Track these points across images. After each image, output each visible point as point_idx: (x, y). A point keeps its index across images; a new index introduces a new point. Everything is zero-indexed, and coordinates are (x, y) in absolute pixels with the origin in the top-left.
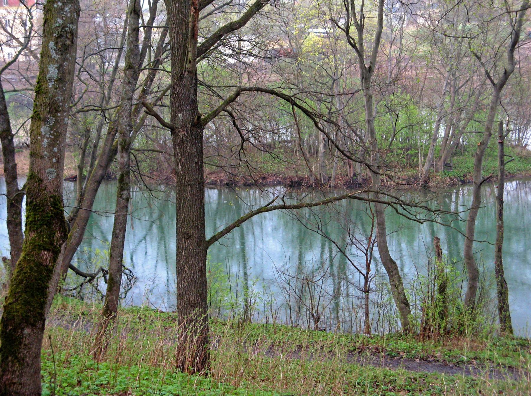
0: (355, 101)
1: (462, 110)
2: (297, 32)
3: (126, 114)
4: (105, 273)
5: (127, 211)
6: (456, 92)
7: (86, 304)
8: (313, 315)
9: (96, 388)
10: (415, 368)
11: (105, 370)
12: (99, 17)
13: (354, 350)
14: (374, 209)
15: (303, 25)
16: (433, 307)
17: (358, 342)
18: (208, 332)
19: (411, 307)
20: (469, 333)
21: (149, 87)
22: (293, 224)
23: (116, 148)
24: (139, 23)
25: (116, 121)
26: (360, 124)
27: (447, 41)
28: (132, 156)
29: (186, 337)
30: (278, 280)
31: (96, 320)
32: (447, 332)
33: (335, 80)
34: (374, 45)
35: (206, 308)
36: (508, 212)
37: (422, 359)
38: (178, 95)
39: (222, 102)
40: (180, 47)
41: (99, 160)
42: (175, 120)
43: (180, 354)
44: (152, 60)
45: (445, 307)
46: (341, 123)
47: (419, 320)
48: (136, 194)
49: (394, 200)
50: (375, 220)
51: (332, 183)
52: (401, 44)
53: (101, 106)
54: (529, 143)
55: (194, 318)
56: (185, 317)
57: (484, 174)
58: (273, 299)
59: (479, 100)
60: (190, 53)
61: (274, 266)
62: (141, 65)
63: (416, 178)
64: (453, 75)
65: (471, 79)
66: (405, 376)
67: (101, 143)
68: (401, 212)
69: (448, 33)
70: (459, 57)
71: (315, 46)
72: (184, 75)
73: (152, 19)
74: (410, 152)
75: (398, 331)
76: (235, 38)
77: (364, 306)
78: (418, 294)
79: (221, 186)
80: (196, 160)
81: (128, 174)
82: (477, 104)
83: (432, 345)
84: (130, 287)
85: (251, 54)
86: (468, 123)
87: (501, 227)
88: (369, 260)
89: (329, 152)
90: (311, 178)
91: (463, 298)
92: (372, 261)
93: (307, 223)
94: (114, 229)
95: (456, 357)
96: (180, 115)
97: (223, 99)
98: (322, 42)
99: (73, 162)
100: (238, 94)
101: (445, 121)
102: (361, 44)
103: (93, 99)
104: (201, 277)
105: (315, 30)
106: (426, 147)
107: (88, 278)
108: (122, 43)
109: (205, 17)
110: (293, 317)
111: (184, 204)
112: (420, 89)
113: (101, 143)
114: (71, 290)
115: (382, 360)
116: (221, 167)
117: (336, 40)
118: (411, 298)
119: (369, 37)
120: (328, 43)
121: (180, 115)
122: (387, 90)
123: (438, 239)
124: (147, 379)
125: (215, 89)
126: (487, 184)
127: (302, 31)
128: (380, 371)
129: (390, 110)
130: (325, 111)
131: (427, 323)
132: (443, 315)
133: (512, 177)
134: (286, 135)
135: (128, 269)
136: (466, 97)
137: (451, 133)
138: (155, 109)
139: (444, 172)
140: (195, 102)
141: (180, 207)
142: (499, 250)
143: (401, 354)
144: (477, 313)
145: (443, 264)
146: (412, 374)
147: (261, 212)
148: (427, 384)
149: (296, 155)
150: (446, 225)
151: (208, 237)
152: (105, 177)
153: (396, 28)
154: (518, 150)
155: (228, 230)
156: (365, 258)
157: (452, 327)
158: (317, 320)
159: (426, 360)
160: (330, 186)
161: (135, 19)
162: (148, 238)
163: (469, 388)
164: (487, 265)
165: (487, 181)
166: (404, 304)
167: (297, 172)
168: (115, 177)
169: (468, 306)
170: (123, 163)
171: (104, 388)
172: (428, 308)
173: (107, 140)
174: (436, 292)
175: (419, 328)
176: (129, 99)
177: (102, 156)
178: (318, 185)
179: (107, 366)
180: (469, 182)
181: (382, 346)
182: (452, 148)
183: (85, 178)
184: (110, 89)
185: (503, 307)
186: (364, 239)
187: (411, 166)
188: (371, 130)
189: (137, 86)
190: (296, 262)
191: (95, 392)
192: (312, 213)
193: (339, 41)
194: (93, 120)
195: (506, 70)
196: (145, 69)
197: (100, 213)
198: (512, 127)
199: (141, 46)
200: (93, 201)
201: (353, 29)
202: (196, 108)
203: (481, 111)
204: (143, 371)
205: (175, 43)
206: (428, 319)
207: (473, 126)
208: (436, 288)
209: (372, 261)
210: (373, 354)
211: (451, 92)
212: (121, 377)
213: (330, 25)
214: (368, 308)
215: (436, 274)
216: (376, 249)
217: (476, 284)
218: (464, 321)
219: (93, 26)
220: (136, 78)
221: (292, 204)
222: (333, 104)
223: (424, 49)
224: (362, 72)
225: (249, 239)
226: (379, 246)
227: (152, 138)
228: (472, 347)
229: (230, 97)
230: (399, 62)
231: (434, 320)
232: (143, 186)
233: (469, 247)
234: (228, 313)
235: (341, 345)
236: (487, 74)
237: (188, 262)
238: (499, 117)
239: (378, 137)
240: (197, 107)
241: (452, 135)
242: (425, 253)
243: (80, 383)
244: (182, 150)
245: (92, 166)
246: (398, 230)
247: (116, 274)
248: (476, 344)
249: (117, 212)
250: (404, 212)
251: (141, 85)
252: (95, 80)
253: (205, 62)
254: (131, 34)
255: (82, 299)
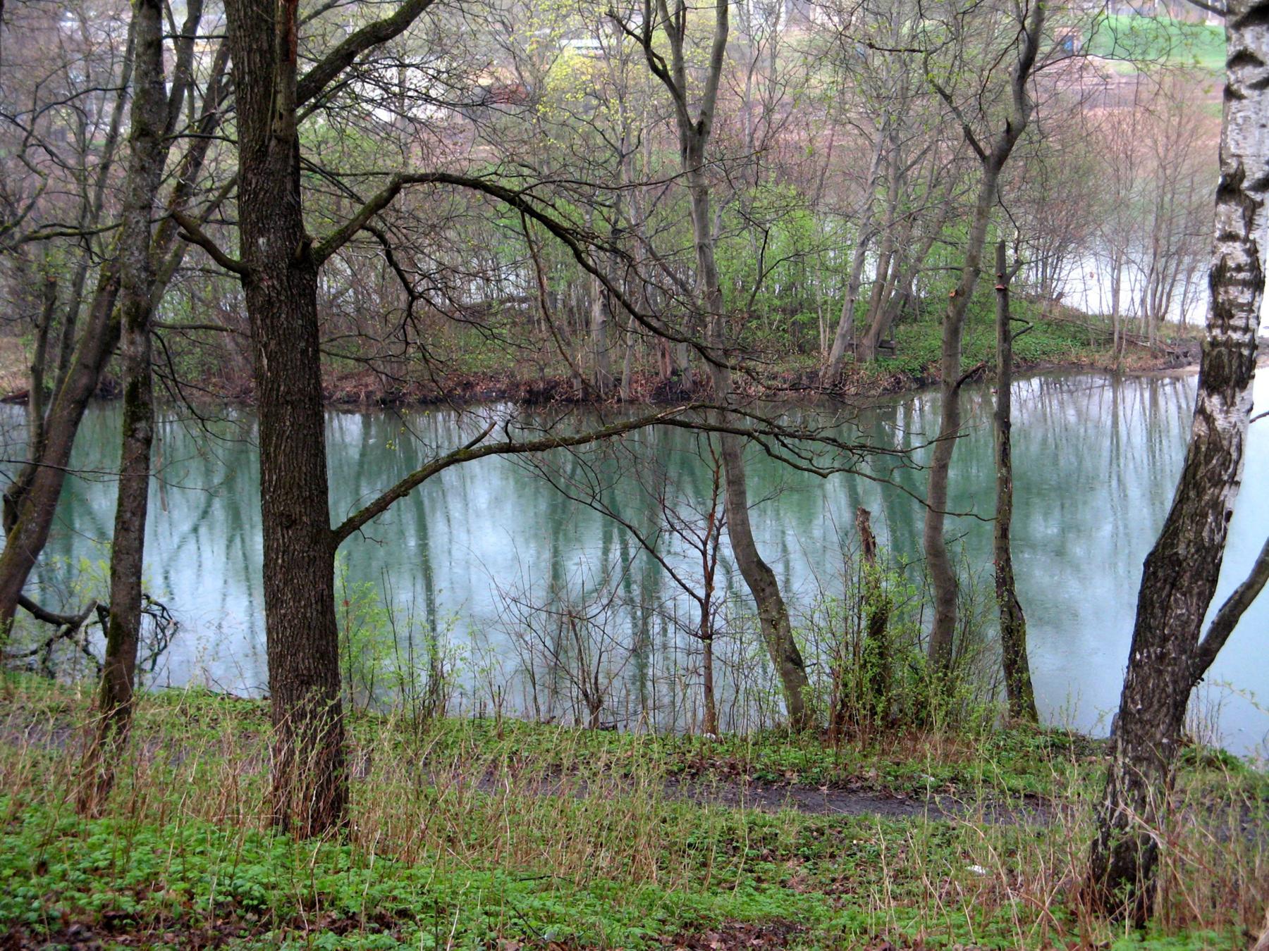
0: (670, 202)
1: (915, 219)
2: (535, 46)
3: (139, 243)
4: (101, 610)
5: (147, 468)
6: (900, 177)
7: (62, 687)
8: (586, 695)
9: (83, 877)
10: (820, 805)
11: (104, 836)
12: (73, 20)
13: (681, 770)
14: (718, 449)
15: (548, 31)
16: (857, 667)
17: (689, 752)
18: (342, 739)
19: (808, 670)
20: (939, 724)
21: (193, 180)
22: (537, 489)
23: (119, 323)
24: (160, 29)
25: (116, 259)
26: (684, 256)
27: (877, 61)
28: (156, 344)
29: (291, 752)
30: (505, 617)
31: (80, 720)
32: (891, 724)
33: (623, 156)
34: (710, 72)
35: (336, 684)
36: (1023, 448)
37: (834, 785)
38: (256, 195)
39: (358, 208)
40: (256, 81)
41: (81, 353)
42: (250, 254)
43: (280, 792)
44: (198, 116)
45: (885, 667)
46: (640, 254)
47: (826, 697)
48: (170, 430)
49: (763, 426)
50: (723, 471)
51: (624, 393)
52: (774, 70)
53: (82, 226)
54: (1066, 290)
55: (308, 709)
56: (288, 707)
57: (965, 363)
58: (494, 661)
59: (953, 195)
60: (279, 96)
61: (493, 585)
62: (170, 126)
63: (813, 375)
64: (892, 139)
65: (933, 148)
66: (797, 823)
67: (84, 311)
68: (777, 453)
69: (877, 42)
70: (904, 97)
71: (576, 79)
72: (268, 146)
73: (194, 19)
74: (798, 317)
75: (779, 724)
76: (389, 62)
77: (702, 671)
78: (823, 640)
79: (368, 405)
80: (303, 344)
81: (147, 382)
82: (947, 203)
83: (856, 754)
84: (163, 644)
85: (428, 99)
86: (930, 246)
87: (1005, 481)
88: (710, 563)
89: (613, 324)
90: (574, 381)
91: (925, 646)
92: (718, 568)
93: (567, 486)
94: (119, 511)
95: (910, 778)
96: (261, 241)
97: (363, 203)
98: (594, 67)
99: (22, 359)
100: (395, 190)
101: (877, 243)
102: (680, 71)
103: (64, 211)
104: (323, 613)
105: (575, 42)
106: (836, 305)
107: (64, 627)
108: (125, 78)
109: (317, 13)
110: (540, 701)
111: (277, 446)
112: (819, 173)
113: (84, 311)
114: (26, 656)
115: (746, 790)
116: (366, 361)
117: (625, 63)
118: (808, 648)
119: (697, 55)
120: (606, 70)
121: (261, 241)
122: (743, 176)
123: (866, 513)
124: (202, 853)
125: (345, 181)
126: (974, 386)
127: (547, 45)
128: (740, 818)
129: (748, 218)
130: (603, 228)
131: (844, 705)
132: (880, 684)
133: (1028, 369)
134: (515, 283)
135: (156, 604)
136: (922, 190)
137: (890, 272)
138: (208, 231)
139: (877, 360)
140: (294, 211)
141: (268, 455)
142: (1004, 533)
143: (788, 775)
144: (958, 677)
145: (878, 568)
146: (813, 820)
147: (458, 461)
148: (847, 841)
149: (541, 331)
150: (885, 482)
151: (335, 524)
152: (98, 391)
153: (759, 33)
154: (1043, 306)
155: (381, 505)
156: (701, 561)
157: (901, 711)
158: (596, 706)
159: (844, 787)
160: (619, 400)
161: (150, 19)
162: (203, 530)
163: (939, 846)
164: (976, 570)
165: (972, 378)
166: (792, 662)
167: (542, 370)
168: (121, 391)
169: (937, 662)
170: (136, 357)
171: (102, 876)
172: (846, 671)
173: (97, 305)
174: (864, 634)
175: (827, 714)
176: (143, 208)
177: (85, 344)
178: (588, 398)
179: (108, 827)
180: (933, 383)
181: (743, 759)
182: (893, 304)
183: (49, 397)
184: (100, 185)
185: (1015, 662)
186: (698, 517)
187: (802, 350)
188: (707, 267)
189: (163, 177)
190: (545, 579)
191: (80, 885)
192: (578, 462)
193: (630, 65)
194: (64, 257)
195: (1009, 124)
196: (182, 136)
197: (84, 475)
198: (1027, 254)
199: (169, 86)
200: (70, 449)
201: (660, 38)
202: (299, 225)
203: (958, 220)
204: (191, 836)
205: (244, 73)
206: (847, 696)
207: (940, 255)
208: (864, 624)
209: (717, 567)
210: (725, 778)
211: (890, 178)
212: (140, 849)
213: (608, 28)
214: (710, 674)
215: (863, 592)
216: (725, 539)
217: (954, 612)
218: (927, 698)
219: (56, 40)
220: (161, 158)
221: (527, 441)
222: (619, 212)
223: (822, 79)
224: (684, 135)
225: (438, 528)
226: (733, 534)
227: (200, 298)
228: (946, 756)
229: (378, 197)
230: (769, 110)
231: (859, 698)
232: (185, 410)
233: (935, 528)
234: (392, 696)
235: (651, 760)
236: (968, 134)
237: (292, 580)
238: (995, 233)
239: (726, 286)
240: (301, 221)
241: (894, 276)
242: (836, 547)
243: (42, 867)
244: (268, 322)
245: (64, 366)
246: (777, 493)
247: (125, 613)
248: (954, 748)
249: (123, 470)
250: (785, 453)
251: (171, 175)
252: (64, 166)
253: (321, 120)
254: (144, 54)
255: (52, 675)
